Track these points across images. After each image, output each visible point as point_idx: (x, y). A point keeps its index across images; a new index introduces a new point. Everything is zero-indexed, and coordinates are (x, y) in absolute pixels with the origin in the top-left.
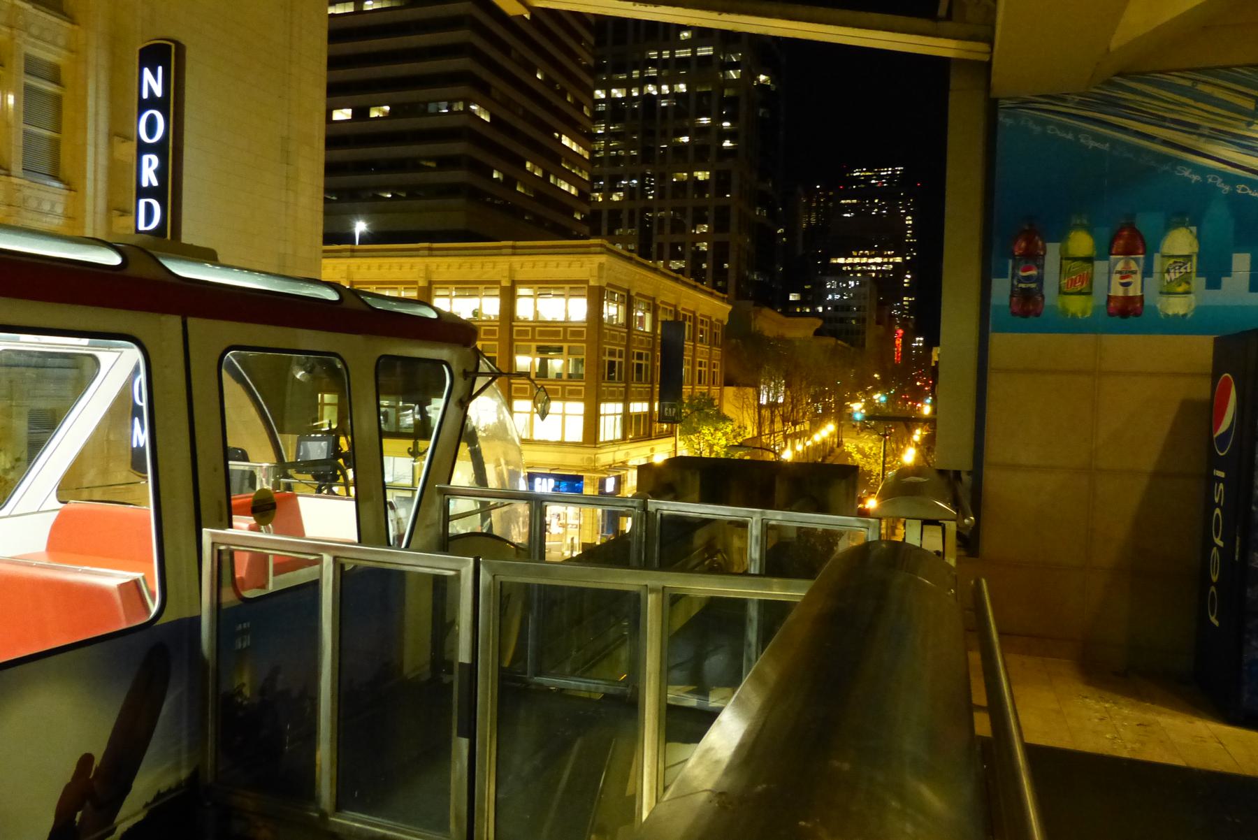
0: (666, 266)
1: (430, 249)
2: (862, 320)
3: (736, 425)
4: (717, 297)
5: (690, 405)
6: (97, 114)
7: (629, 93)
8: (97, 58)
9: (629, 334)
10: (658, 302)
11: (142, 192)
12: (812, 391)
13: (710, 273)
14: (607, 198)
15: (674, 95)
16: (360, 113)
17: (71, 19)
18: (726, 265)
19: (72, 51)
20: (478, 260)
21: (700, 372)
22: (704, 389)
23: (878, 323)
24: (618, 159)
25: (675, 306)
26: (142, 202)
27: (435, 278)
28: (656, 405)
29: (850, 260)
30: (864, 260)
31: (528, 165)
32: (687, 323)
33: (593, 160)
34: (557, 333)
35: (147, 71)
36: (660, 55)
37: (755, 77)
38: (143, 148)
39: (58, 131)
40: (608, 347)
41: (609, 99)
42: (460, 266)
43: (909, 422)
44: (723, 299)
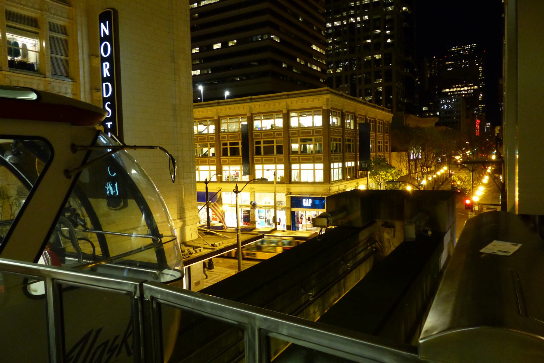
0: (363, 99)
1: (251, 99)
3: (397, 170)
4: (386, 111)
5: (374, 162)
7: (342, 23)
8: (81, 20)
9: (343, 130)
10: (367, 117)
11: (105, 80)
12: (435, 152)
14: (335, 71)
15: (363, 21)
16: (225, 45)
17: (69, 5)
20: (271, 102)
22: (381, 154)
23: (467, 118)
26: (104, 84)
27: (254, 112)
28: (358, 162)
29: (452, 90)
30: (459, 89)
31: (298, 60)
32: (372, 124)
33: (327, 55)
34: (309, 132)
35: (102, 24)
36: (355, 4)
38: (103, 60)
39: (67, 56)
40: (333, 137)
41: (334, 27)
42: (264, 106)
43: (485, 163)
44: (388, 112)
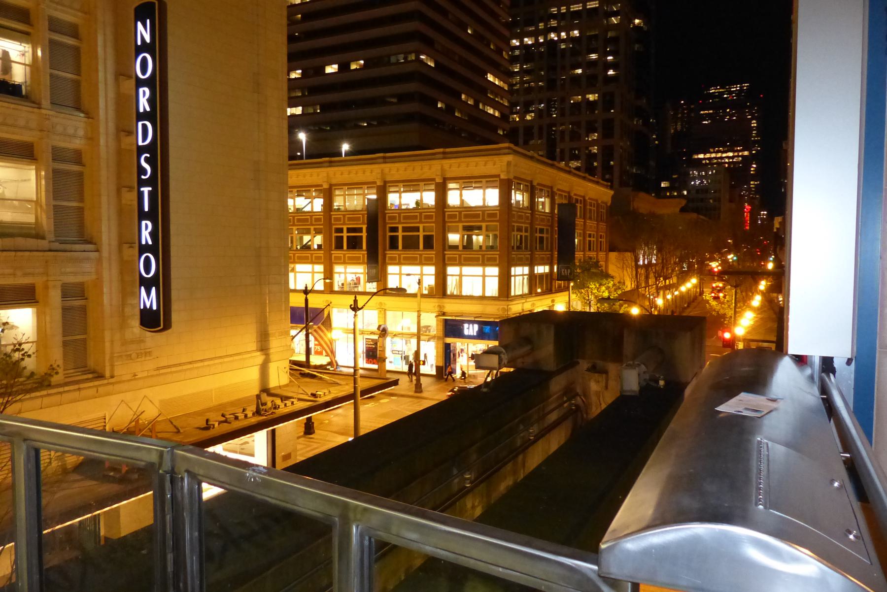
2: (718, 200)
6: (105, 59)
7: (537, 40)
9: (532, 214)
10: (555, 190)
11: (141, 117)
12: (678, 254)
13: (599, 170)
14: (522, 118)
15: (570, 39)
18: (612, 163)
19: (86, 13)
21: (590, 241)
23: (731, 201)
24: (529, 90)
25: (569, 193)
27: (388, 179)
28: (555, 267)
29: (708, 156)
30: (719, 155)
31: (463, 97)
32: (578, 205)
33: (511, 92)
34: (477, 216)
35: (139, 24)
36: (559, 10)
37: (631, 21)
38: (140, 83)
39: (79, 75)
40: (516, 225)
41: (523, 46)
43: (757, 275)
44: (606, 187)
